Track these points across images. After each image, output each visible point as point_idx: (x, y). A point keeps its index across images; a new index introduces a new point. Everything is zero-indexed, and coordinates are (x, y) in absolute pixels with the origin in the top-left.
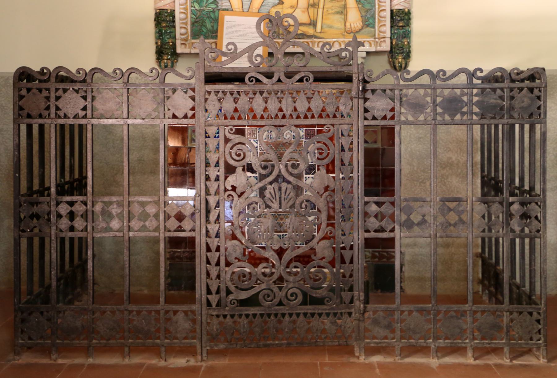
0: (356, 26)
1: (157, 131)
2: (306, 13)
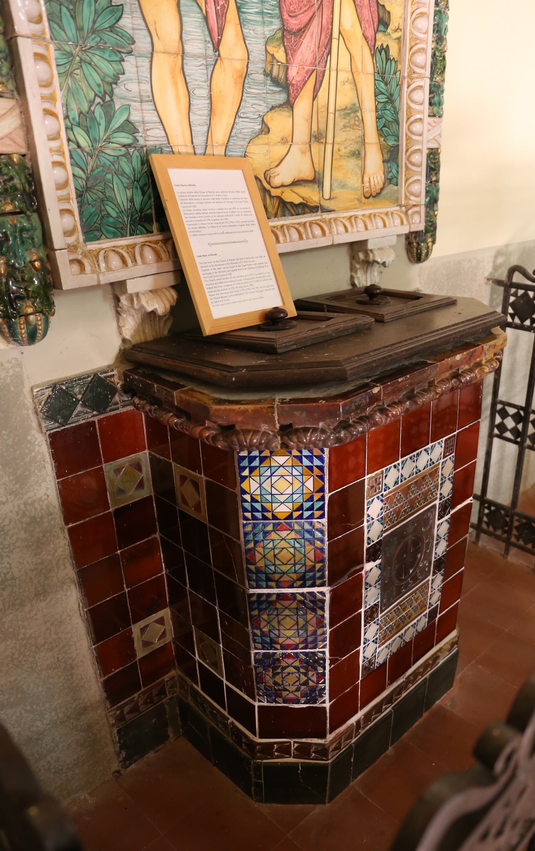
0: (376, 182)
1: (29, 501)
2: (308, 154)
